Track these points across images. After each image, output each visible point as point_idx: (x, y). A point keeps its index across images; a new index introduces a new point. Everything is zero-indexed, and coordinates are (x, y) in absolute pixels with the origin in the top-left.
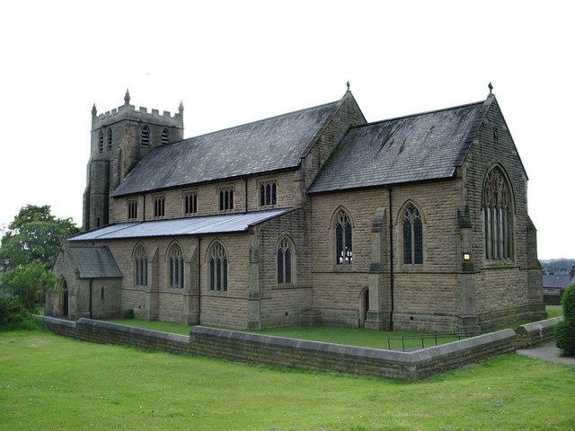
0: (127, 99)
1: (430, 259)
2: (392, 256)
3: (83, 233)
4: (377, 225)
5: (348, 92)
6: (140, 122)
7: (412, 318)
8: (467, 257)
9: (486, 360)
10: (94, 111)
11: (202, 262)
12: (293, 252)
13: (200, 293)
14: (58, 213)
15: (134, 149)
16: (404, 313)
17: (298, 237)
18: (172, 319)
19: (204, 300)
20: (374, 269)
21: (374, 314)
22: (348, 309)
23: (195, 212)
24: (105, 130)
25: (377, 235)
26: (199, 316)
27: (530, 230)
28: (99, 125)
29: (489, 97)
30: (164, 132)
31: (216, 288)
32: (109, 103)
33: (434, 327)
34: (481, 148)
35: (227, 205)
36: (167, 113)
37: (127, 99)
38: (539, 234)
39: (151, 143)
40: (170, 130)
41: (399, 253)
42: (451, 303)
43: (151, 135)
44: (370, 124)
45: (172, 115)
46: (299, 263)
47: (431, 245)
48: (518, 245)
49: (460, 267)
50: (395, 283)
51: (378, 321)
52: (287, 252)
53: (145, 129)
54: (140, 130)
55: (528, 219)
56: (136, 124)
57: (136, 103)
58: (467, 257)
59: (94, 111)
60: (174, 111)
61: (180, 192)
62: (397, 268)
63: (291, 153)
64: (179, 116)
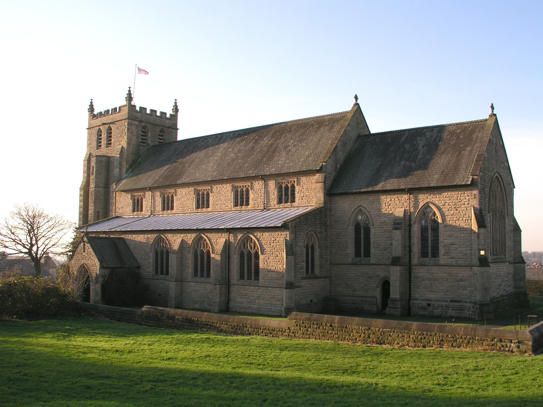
0: (130, 98)
1: (447, 253)
2: (410, 251)
3: (93, 224)
4: (398, 224)
5: (357, 104)
6: (141, 121)
7: (429, 305)
8: (482, 253)
9: (342, 384)
10: (91, 109)
11: (232, 254)
12: (317, 247)
13: (229, 282)
14: (475, 203)
15: (141, 147)
16: (420, 300)
17: (321, 232)
18: (197, 306)
19: (233, 289)
20: (395, 261)
21: (394, 300)
22: (366, 297)
23: (172, 209)
24: (101, 126)
25: (398, 232)
26: (228, 303)
27: (517, 230)
28: (98, 122)
29: (491, 116)
30: (160, 131)
31: (253, 277)
32: (111, 100)
33: (451, 312)
34: (477, 155)
35: (203, 204)
36: (163, 114)
37: (130, 98)
38: (523, 234)
39: (149, 142)
40: (165, 130)
41: (416, 248)
42: (465, 292)
43: (149, 134)
44: (374, 134)
45: (168, 116)
46: (321, 255)
47: (448, 241)
48: (509, 243)
49: (476, 262)
50: (412, 274)
51: (399, 306)
52: (312, 245)
53: (144, 128)
54: (140, 129)
55: (515, 221)
56: (137, 123)
57: (138, 103)
58: (482, 253)
59: (91, 109)
60: (169, 112)
61: (192, 189)
62: (415, 261)
63: (308, 157)
64: (174, 117)
